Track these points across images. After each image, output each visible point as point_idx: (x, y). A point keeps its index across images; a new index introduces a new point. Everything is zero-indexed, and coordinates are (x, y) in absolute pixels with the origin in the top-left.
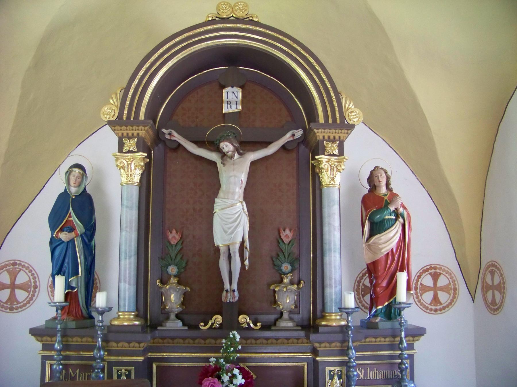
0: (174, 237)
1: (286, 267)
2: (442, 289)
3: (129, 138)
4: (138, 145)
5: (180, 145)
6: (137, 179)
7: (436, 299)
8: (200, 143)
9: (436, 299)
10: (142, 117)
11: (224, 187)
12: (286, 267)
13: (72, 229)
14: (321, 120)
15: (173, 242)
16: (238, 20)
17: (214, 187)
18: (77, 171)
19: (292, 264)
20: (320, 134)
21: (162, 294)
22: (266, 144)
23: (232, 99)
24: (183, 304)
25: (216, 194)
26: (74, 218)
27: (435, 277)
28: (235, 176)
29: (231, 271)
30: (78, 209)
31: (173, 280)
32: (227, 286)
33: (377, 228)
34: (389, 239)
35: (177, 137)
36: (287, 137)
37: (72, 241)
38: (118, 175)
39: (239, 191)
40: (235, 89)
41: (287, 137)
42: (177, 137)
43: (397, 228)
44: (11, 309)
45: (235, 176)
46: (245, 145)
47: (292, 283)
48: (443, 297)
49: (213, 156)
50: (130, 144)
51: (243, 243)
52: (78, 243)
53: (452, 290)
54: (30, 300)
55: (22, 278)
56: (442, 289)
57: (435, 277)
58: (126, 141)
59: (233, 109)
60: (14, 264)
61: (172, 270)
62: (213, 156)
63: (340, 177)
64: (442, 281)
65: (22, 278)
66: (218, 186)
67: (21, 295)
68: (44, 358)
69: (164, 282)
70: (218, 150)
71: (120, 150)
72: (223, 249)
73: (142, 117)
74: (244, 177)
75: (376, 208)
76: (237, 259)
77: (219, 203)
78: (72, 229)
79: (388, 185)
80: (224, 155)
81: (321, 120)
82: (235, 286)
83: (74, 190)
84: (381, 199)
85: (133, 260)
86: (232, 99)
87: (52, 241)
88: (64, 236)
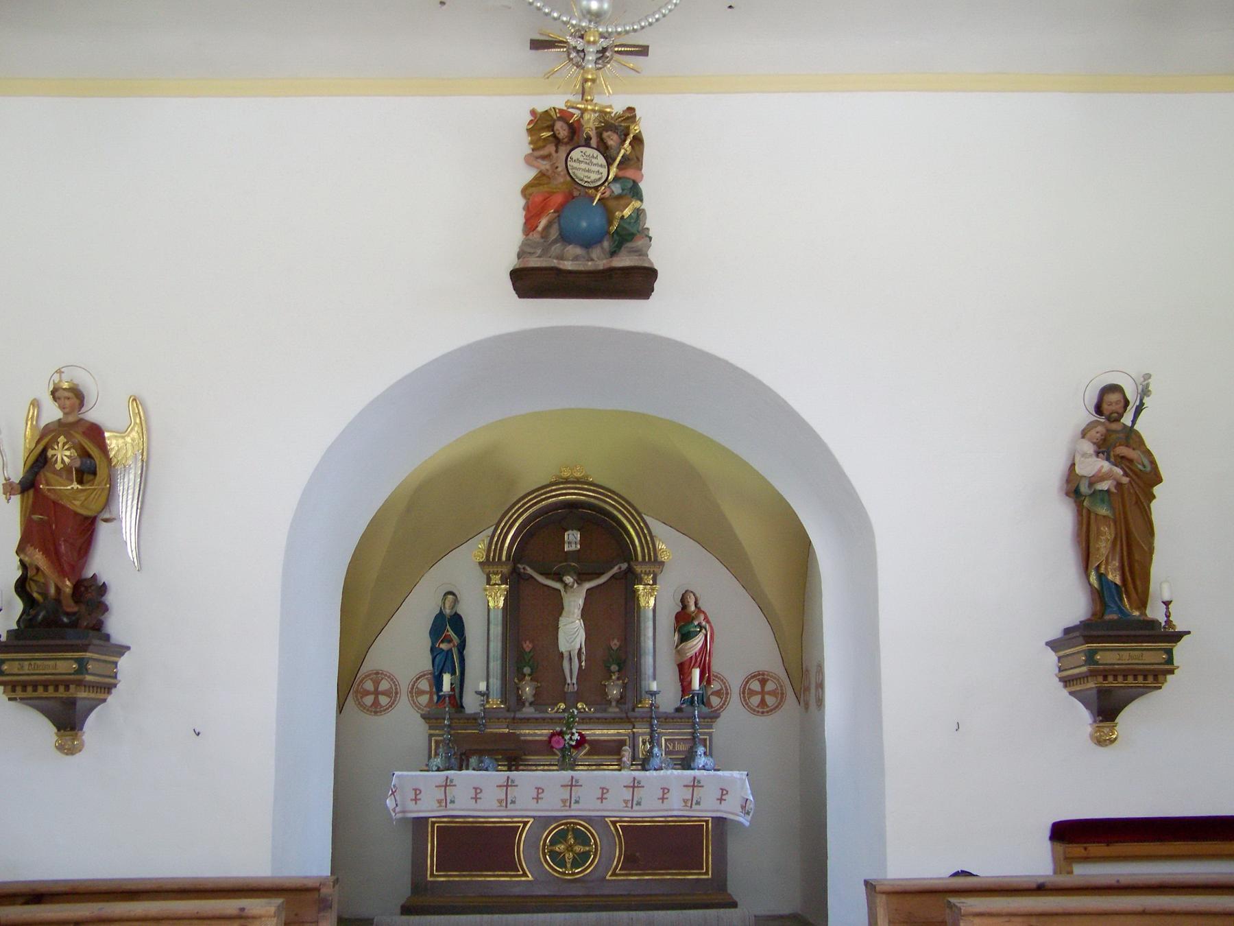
0: (527, 646)
1: (527, 670)
2: (769, 693)
3: (496, 574)
4: (501, 579)
5: (532, 577)
6: (501, 604)
7: (763, 703)
8: (546, 575)
9: (763, 703)
10: (504, 558)
11: (566, 608)
12: (614, 668)
13: (450, 641)
14: (640, 559)
15: (527, 650)
16: (578, 481)
17: (559, 609)
18: (450, 597)
19: (619, 665)
20: (638, 569)
21: (518, 689)
22: (599, 575)
23: (572, 540)
24: (534, 696)
25: (560, 614)
26: (451, 633)
27: (763, 682)
28: (575, 602)
29: (571, 670)
30: (448, 627)
31: (527, 678)
32: (569, 681)
33: (685, 637)
34: (696, 643)
35: (529, 571)
36: (616, 569)
37: (451, 650)
38: (485, 603)
39: (578, 612)
40: (575, 532)
41: (616, 569)
42: (529, 571)
43: (701, 637)
44: (376, 713)
45: (575, 602)
46: (582, 577)
47: (618, 679)
48: (770, 700)
49: (557, 585)
50: (496, 579)
51: (580, 649)
52: (455, 651)
53: (780, 695)
54: (391, 705)
55: (384, 686)
56: (769, 693)
57: (763, 682)
58: (493, 577)
59: (573, 548)
60: (377, 673)
61: (527, 670)
62: (557, 585)
63: (656, 601)
64: (770, 686)
65: (384, 686)
66: (563, 608)
67: (384, 700)
68: (431, 736)
69: (521, 680)
70: (561, 581)
71: (488, 583)
72: (566, 655)
73: (504, 558)
74: (581, 602)
75: (686, 621)
76: (576, 660)
77: (563, 621)
78: (450, 641)
79: (696, 604)
80: (566, 585)
81: (640, 559)
82: (574, 681)
83: (448, 611)
84: (689, 615)
85: (499, 662)
86: (572, 540)
87: (432, 650)
88: (444, 646)
